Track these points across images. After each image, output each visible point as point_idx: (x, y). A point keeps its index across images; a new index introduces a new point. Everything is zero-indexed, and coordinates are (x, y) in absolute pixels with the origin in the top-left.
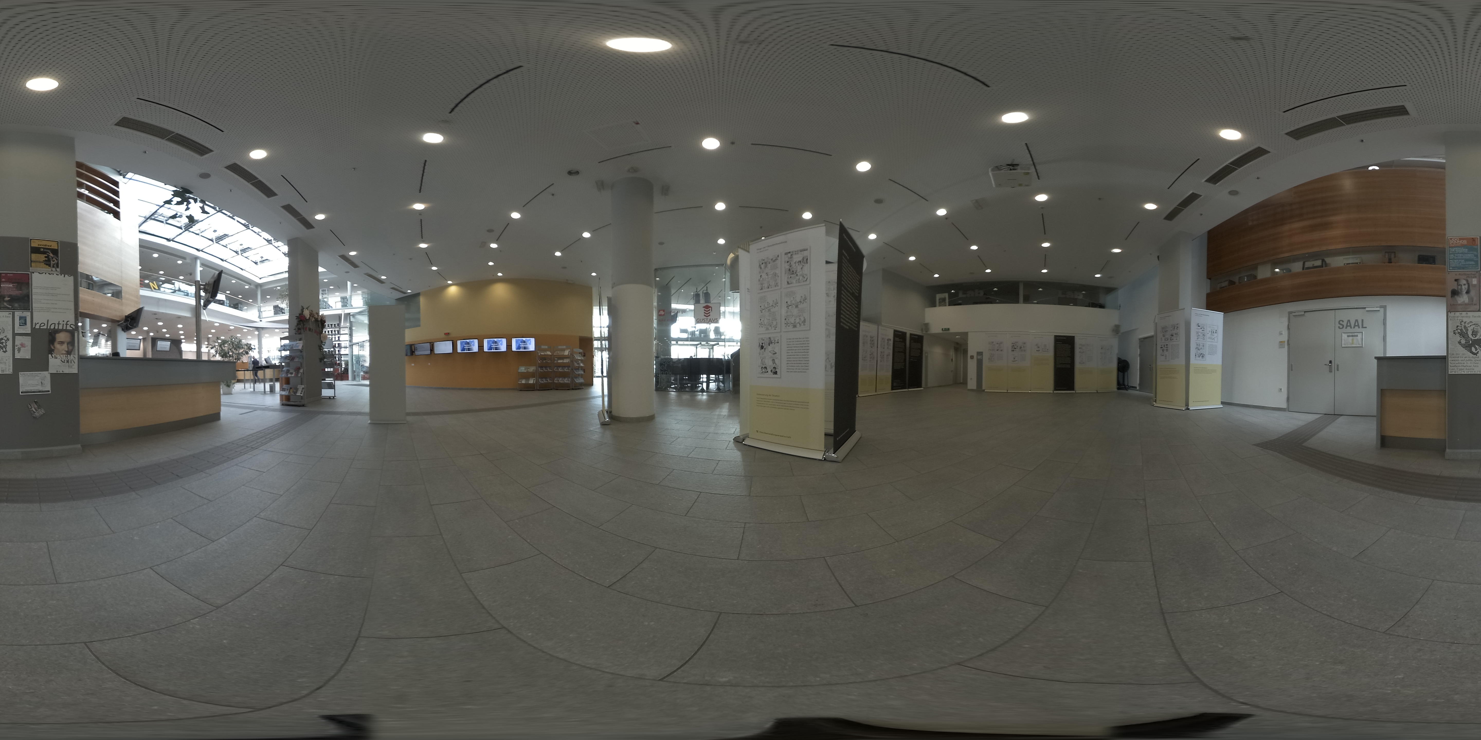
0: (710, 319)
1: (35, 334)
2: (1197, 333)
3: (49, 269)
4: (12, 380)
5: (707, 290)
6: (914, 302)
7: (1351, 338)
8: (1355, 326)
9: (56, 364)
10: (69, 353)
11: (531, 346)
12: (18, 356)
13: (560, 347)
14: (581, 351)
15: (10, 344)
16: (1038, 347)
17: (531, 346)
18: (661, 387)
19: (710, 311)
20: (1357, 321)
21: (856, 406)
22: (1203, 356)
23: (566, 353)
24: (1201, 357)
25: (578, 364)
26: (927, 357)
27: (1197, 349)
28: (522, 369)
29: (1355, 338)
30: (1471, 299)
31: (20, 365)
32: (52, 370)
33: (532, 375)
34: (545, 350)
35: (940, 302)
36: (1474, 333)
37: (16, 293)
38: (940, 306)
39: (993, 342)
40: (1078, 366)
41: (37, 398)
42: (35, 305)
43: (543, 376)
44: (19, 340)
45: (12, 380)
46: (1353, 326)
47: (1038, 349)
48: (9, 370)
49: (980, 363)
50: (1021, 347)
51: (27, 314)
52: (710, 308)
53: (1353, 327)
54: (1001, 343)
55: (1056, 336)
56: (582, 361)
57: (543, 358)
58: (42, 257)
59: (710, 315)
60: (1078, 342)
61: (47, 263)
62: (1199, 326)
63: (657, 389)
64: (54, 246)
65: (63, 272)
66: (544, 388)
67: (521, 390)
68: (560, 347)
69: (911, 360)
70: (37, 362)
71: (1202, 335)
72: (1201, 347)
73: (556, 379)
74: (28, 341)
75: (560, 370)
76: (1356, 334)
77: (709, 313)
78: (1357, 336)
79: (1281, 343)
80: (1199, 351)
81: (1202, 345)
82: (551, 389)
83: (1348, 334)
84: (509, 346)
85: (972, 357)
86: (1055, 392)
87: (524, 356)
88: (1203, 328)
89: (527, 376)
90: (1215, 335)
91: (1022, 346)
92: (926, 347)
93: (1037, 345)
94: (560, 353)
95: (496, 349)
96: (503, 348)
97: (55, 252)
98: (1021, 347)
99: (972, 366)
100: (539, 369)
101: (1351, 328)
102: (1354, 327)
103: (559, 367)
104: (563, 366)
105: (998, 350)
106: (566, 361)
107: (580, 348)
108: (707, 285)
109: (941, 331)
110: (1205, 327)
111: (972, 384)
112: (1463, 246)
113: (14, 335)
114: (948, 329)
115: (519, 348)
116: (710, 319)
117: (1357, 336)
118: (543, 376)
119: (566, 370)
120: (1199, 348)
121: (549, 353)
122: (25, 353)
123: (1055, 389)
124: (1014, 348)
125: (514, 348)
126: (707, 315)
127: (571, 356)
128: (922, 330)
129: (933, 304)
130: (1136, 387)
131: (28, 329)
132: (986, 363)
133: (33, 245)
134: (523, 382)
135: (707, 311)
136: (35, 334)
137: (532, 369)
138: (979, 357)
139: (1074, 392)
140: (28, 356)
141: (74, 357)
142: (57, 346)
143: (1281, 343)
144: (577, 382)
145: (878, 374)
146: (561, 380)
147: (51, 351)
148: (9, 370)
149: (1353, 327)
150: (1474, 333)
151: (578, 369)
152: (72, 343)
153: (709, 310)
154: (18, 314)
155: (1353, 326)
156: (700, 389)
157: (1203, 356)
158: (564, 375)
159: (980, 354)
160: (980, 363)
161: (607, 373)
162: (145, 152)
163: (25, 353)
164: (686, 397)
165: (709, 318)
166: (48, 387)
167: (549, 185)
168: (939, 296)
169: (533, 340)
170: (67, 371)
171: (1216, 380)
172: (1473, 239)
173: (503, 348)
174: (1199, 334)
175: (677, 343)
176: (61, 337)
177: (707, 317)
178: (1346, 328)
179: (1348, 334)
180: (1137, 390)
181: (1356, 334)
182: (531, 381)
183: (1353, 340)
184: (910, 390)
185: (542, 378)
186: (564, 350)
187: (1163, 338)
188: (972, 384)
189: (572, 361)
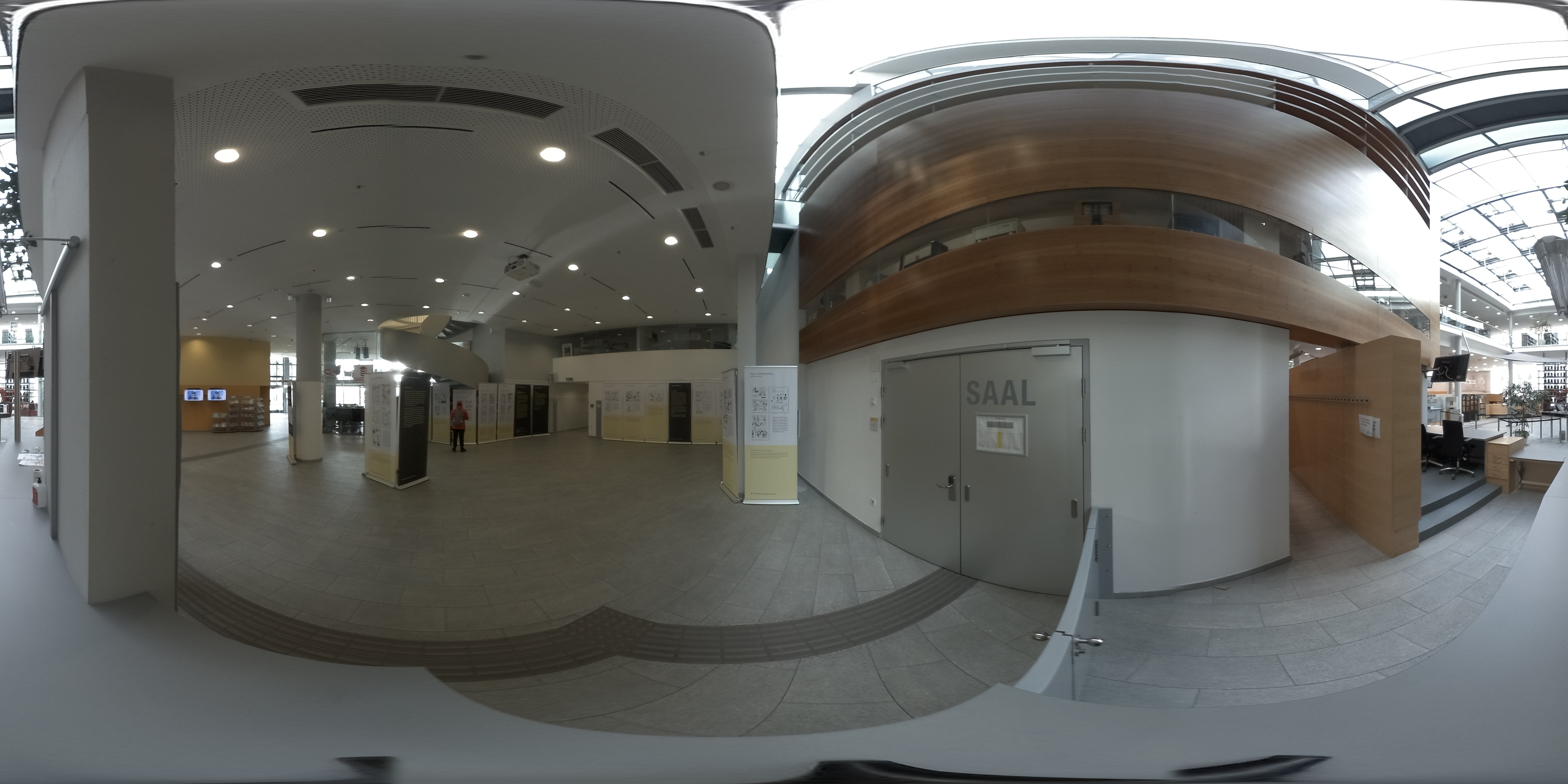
2: (754, 402)
5: (366, 345)
6: (540, 354)
7: (995, 430)
8: (1005, 398)
11: (223, 397)
13: (246, 397)
14: (262, 399)
16: (653, 397)
17: (223, 397)
18: (327, 430)
20: (1009, 383)
22: (764, 435)
23: (251, 402)
24: (761, 436)
25: (261, 410)
26: (555, 405)
27: (754, 425)
28: (216, 415)
29: (1005, 430)
33: (224, 420)
34: (234, 400)
35: (565, 352)
38: (565, 356)
39: (609, 392)
40: (694, 415)
43: (232, 421)
46: (1000, 398)
49: (599, 411)
50: (635, 397)
53: (1000, 400)
54: (617, 392)
56: (263, 407)
57: (233, 406)
60: (694, 389)
62: (757, 392)
63: (324, 432)
66: (233, 430)
67: (215, 433)
68: (246, 397)
69: (536, 409)
71: (762, 404)
72: (761, 422)
73: (242, 423)
75: (246, 415)
76: (1008, 420)
78: (1010, 426)
80: (758, 427)
81: (762, 419)
82: (238, 431)
84: (205, 396)
85: (592, 406)
86: (669, 443)
87: (217, 404)
88: (762, 394)
89: (219, 421)
90: (785, 401)
91: (636, 396)
92: (551, 395)
93: (651, 394)
94: (246, 402)
95: (195, 398)
96: (201, 398)
98: (635, 397)
99: (592, 414)
100: (230, 415)
101: (996, 403)
102: (1003, 403)
103: (246, 413)
104: (249, 412)
105: (613, 400)
106: (251, 408)
107: (261, 397)
108: (366, 341)
109: (566, 381)
110: (767, 392)
111: (592, 432)
114: (572, 379)
115: (213, 398)
117: (1010, 426)
118: (232, 421)
119: (251, 416)
120: (758, 423)
121: (237, 402)
124: (628, 398)
125: (209, 398)
127: (255, 405)
128: (549, 380)
129: (560, 355)
132: (604, 412)
134: (217, 426)
137: (224, 415)
138: (598, 406)
139: (690, 443)
144: (259, 425)
145: (498, 424)
146: (246, 424)
149: (1000, 400)
151: (259, 414)
155: (1000, 398)
156: (358, 431)
157: (764, 435)
158: (249, 420)
159: (599, 402)
160: (599, 411)
164: (348, 439)
168: (564, 346)
169: (224, 392)
171: (790, 468)
173: (201, 398)
174: (758, 403)
178: (985, 402)
181: (1008, 420)
182: (223, 425)
183: (1000, 435)
184: (533, 436)
185: (231, 422)
186: (249, 399)
188: (592, 432)
189: (255, 409)
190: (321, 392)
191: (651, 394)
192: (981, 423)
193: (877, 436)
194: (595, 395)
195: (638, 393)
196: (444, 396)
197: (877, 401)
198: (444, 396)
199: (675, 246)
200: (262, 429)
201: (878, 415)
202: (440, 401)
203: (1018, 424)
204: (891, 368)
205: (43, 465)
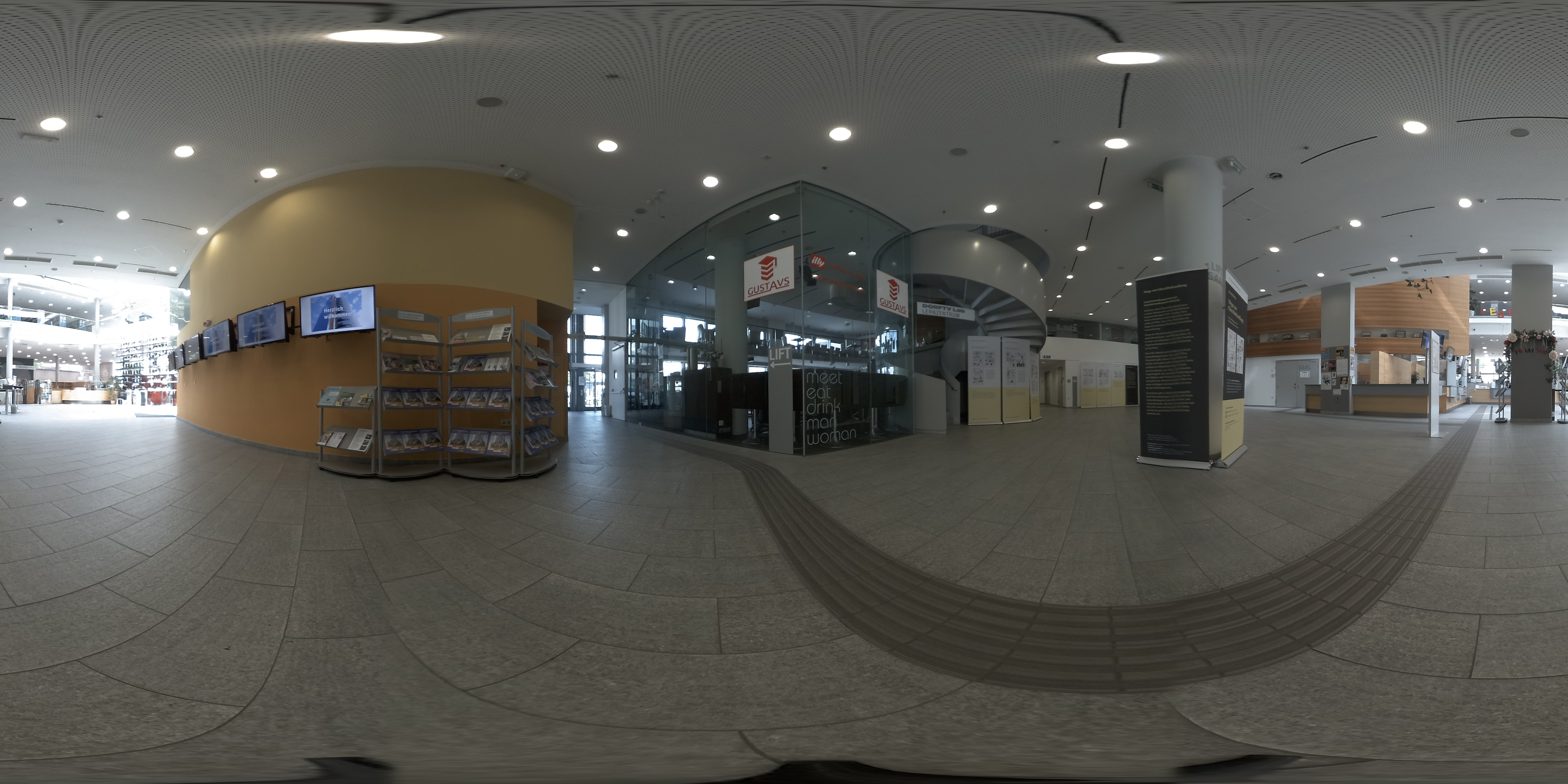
0: (773, 282)
1: (1337, 378)
3: (1341, 357)
4: (1331, 391)
9: (1342, 387)
10: (1346, 384)
13: (470, 316)
19: (773, 266)
21: (1141, 436)
31: (1333, 387)
32: (1340, 390)
37: (1332, 366)
42: (1337, 370)
45: (1331, 391)
48: (1331, 389)
49: (1075, 386)
50: (1105, 374)
51: (1335, 373)
52: (774, 261)
54: (1092, 370)
58: (1339, 353)
59: (772, 275)
61: (1341, 355)
64: (1342, 348)
65: (1345, 358)
68: (470, 316)
70: (1338, 387)
73: (454, 436)
74: (1335, 380)
77: (772, 270)
85: (1069, 381)
93: (1115, 372)
97: (1343, 351)
99: (1069, 388)
113: (1332, 379)
114: (1050, 357)
116: (773, 282)
122: (1335, 384)
124: (1101, 374)
126: (767, 276)
131: (1335, 377)
133: (1337, 349)
135: (767, 269)
136: (1337, 378)
138: (1075, 381)
140: (1335, 385)
147: (1341, 383)
148: (1331, 389)
152: (1347, 380)
153: (772, 265)
154: (1333, 373)
159: (1075, 378)
161: (775, 351)
162: (32, 229)
163: (1335, 384)
165: (771, 281)
167: (1117, 118)
170: (1345, 389)
172: (1327, 349)
175: (1470, 365)
176: (1344, 379)
177: (767, 279)
188: (1069, 403)
190: (1148, 290)
191: (1115, 372)
192: (1301, 373)
193: (1274, 379)
194: (1070, 371)
195: (1108, 371)
196: (1022, 357)
197: (1274, 370)
198: (1022, 357)
199: (175, 148)
200: (308, 763)
201: (1274, 372)
202: (1016, 363)
203: (1308, 372)
204: (1277, 362)
205: (399, 312)
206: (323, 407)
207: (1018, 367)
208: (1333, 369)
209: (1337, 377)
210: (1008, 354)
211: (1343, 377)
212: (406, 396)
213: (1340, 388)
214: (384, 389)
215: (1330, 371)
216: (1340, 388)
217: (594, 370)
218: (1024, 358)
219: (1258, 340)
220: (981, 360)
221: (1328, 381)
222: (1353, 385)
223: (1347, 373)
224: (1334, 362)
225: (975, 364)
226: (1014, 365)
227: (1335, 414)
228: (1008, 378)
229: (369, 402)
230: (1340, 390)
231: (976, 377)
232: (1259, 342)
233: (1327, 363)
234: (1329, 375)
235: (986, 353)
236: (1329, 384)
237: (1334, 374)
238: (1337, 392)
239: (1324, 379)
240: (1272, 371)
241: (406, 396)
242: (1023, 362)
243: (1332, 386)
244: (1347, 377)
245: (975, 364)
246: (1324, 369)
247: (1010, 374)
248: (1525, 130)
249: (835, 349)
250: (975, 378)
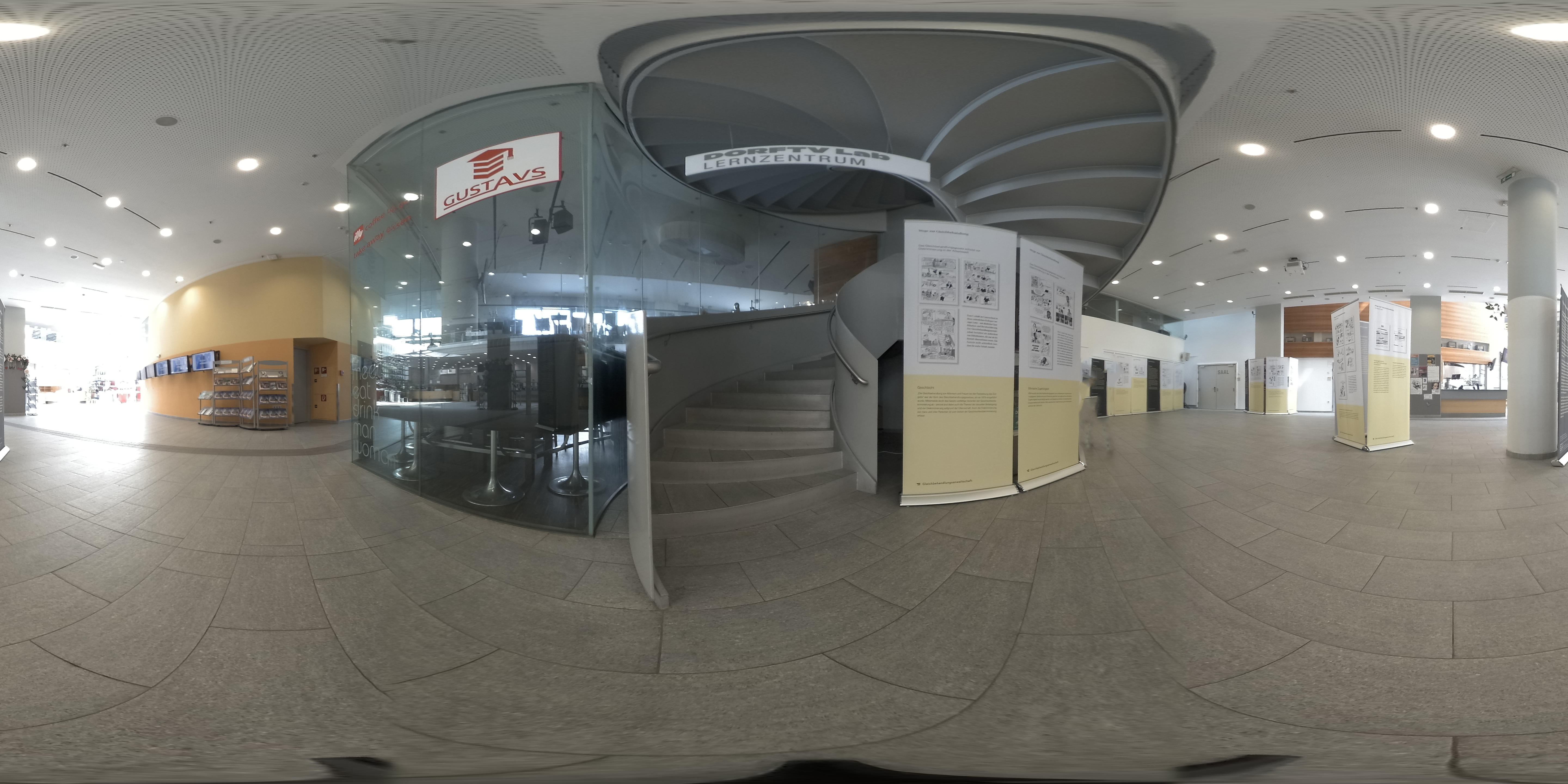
1: (1428, 383)
3: (1432, 364)
4: (1422, 396)
9: (1434, 392)
10: (1437, 389)
12: (1423, 390)
15: (1421, 387)
16: (1137, 370)
30: (1416, 374)
31: (1424, 392)
32: (1431, 395)
36: (1417, 384)
37: (1423, 372)
40: (1162, 388)
41: (1428, 401)
42: (1428, 376)
44: (1424, 385)
45: (1422, 396)
47: (1137, 371)
48: (1421, 393)
51: (1426, 378)
55: (1149, 360)
58: (1430, 361)
61: (1432, 363)
70: (1429, 392)
79: (1329, 378)
83: (662, 312)
86: (1149, 412)
97: (1434, 358)
112: (1415, 358)
113: (1423, 384)
122: (1426, 389)
123: (1148, 410)
130: (1195, 406)
131: (1426, 383)
136: (1428, 383)
140: (1426, 390)
141: (1439, 390)
142: (1434, 387)
143: (1329, 378)
147: (1432, 389)
148: (1421, 393)
150: (1417, 384)
152: (1438, 386)
154: (1424, 378)
163: (1426, 389)
166: (1431, 398)
170: (1437, 394)
172: (1417, 355)
176: (1435, 384)
179: (662, 312)
180: (1196, 408)
187: (1272, 373)
193: (1331, 383)
197: (1331, 373)
201: (1331, 375)
206: (201, 399)
207: (1059, 323)
208: (1424, 374)
209: (1428, 382)
210: (1035, 282)
211: (1435, 383)
212: (270, 398)
213: (1431, 393)
214: (215, 393)
215: (1420, 377)
216: (1431, 393)
217: (832, 427)
218: (1071, 301)
219: (1311, 339)
220: (950, 286)
221: (1418, 386)
222: (1442, 390)
223: (1439, 380)
224: (1425, 369)
225: (928, 295)
226: (1049, 316)
227: (1426, 417)
228: (1035, 349)
229: (1562, 415)
230: (1431, 395)
231: (932, 338)
232: (1313, 341)
233: (1417, 369)
234: (1420, 380)
235: (968, 265)
236: (1419, 389)
237: (1425, 380)
238: (1428, 397)
239: (1414, 384)
240: (1328, 373)
241: (270, 398)
242: (1069, 313)
243: (1423, 391)
244: (1438, 383)
245: (928, 295)
246: (1414, 374)
247: (1040, 338)
248: (1252, 205)
249: (488, 435)
250: (927, 343)
